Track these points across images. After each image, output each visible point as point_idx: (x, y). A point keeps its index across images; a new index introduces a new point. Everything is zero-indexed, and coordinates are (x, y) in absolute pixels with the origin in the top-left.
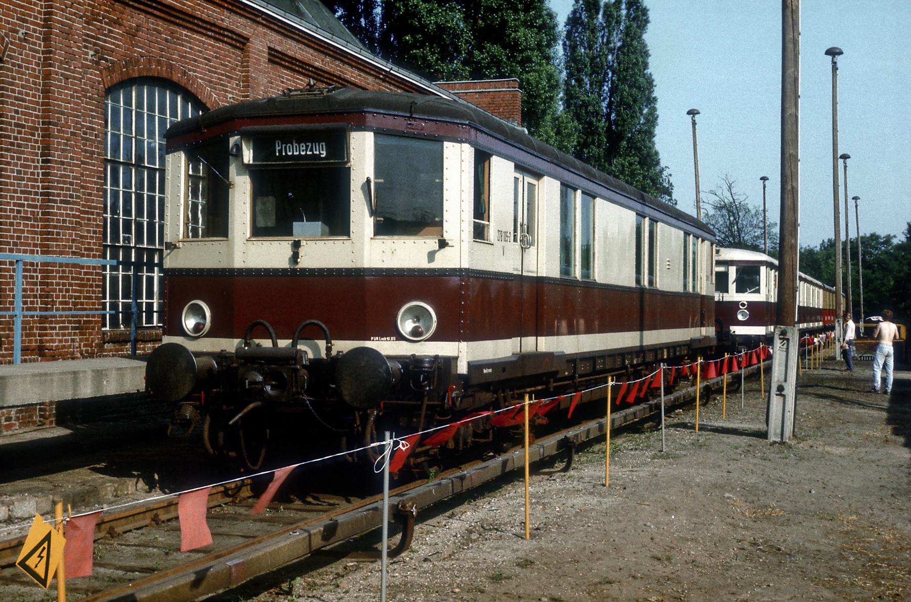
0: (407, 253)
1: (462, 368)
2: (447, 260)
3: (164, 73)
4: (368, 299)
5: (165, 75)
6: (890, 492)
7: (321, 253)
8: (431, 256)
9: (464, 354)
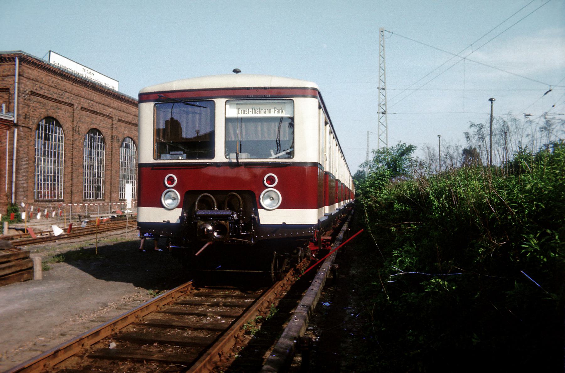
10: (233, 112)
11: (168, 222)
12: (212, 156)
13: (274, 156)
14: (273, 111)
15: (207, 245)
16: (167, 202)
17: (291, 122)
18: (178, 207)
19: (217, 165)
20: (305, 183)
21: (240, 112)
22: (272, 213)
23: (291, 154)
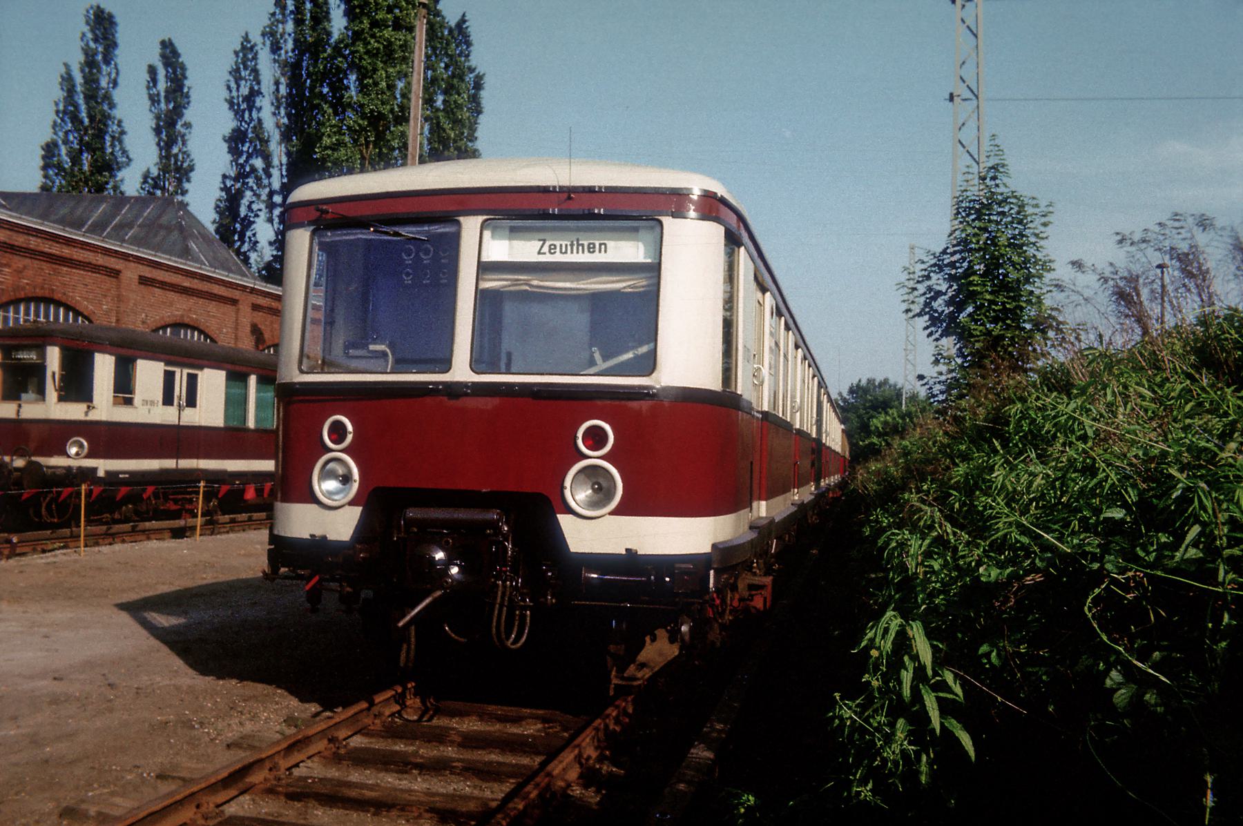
0: (74, 411)
1: (101, 473)
2: (94, 416)
3: (47, 294)
4: (56, 435)
5: (47, 295)
6: (1157, 258)
7: (32, 410)
8: (86, 414)
9: (103, 466)
10: (500, 249)
11: (324, 537)
12: (445, 364)
13: (602, 365)
14: (627, 250)
15: (427, 601)
16: (326, 487)
17: (654, 269)
18: (352, 503)
19: (454, 390)
20: (689, 447)
21: (546, 249)
22: (596, 529)
23: (649, 364)
